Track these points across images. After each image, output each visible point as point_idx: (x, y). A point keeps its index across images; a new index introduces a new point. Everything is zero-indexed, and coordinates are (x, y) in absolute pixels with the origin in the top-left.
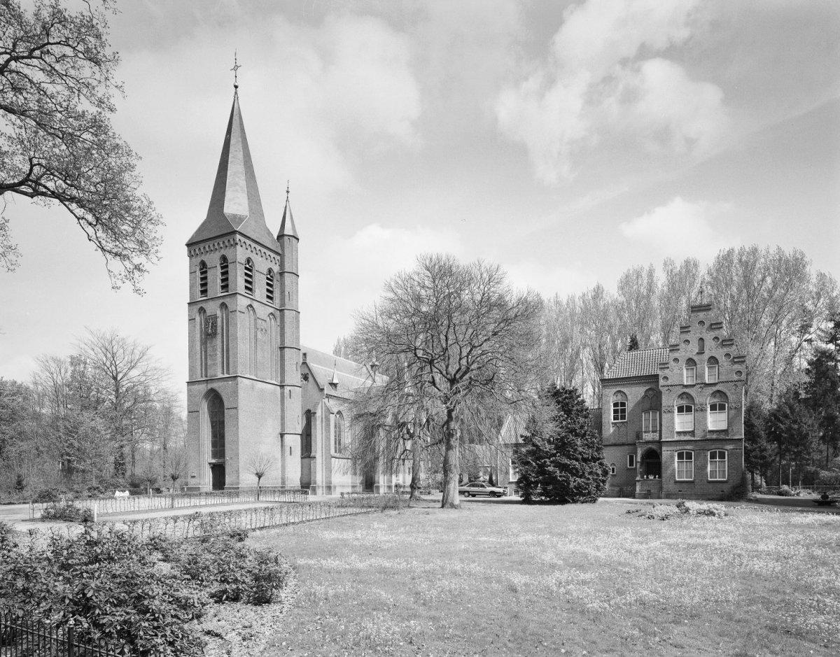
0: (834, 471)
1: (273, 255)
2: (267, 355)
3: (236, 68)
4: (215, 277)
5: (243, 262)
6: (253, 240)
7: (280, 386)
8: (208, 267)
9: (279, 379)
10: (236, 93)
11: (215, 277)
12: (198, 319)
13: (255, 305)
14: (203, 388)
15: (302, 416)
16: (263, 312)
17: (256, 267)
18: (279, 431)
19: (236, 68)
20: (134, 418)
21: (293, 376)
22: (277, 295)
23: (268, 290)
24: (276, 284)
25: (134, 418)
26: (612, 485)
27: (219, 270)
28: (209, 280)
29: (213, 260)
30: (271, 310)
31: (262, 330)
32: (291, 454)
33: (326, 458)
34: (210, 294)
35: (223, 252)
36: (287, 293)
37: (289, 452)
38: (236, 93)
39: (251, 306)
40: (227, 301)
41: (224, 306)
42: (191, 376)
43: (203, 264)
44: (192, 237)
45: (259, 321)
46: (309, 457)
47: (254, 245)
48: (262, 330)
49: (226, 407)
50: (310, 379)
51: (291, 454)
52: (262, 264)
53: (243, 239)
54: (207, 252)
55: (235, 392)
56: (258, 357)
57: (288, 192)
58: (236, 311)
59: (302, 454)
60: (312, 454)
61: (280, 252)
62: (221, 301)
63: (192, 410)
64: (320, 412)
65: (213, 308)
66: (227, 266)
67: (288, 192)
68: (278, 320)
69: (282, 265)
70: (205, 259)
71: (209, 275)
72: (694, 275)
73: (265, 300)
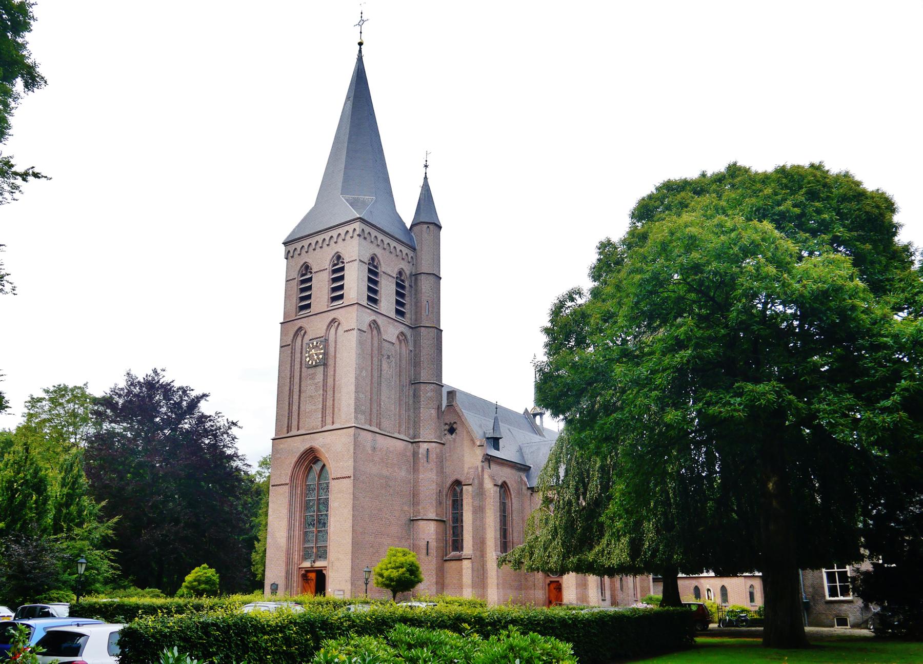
0: (23, 624)
3: (362, 22)
5: (366, 261)
6: (379, 229)
10: (360, 51)
11: (321, 285)
12: (401, 570)
13: (381, 321)
19: (362, 22)
26: (790, 402)
29: (321, 261)
30: (402, 328)
31: (388, 357)
37: (425, 551)
38: (360, 51)
43: (306, 268)
44: (294, 231)
45: (385, 344)
47: (380, 237)
48: (388, 357)
52: (390, 267)
56: (383, 398)
57: (426, 166)
62: (332, 315)
63: (458, 562)
67: (426, 166)
70: (310, 261)
72: (763, 240)
73: (393, 314)
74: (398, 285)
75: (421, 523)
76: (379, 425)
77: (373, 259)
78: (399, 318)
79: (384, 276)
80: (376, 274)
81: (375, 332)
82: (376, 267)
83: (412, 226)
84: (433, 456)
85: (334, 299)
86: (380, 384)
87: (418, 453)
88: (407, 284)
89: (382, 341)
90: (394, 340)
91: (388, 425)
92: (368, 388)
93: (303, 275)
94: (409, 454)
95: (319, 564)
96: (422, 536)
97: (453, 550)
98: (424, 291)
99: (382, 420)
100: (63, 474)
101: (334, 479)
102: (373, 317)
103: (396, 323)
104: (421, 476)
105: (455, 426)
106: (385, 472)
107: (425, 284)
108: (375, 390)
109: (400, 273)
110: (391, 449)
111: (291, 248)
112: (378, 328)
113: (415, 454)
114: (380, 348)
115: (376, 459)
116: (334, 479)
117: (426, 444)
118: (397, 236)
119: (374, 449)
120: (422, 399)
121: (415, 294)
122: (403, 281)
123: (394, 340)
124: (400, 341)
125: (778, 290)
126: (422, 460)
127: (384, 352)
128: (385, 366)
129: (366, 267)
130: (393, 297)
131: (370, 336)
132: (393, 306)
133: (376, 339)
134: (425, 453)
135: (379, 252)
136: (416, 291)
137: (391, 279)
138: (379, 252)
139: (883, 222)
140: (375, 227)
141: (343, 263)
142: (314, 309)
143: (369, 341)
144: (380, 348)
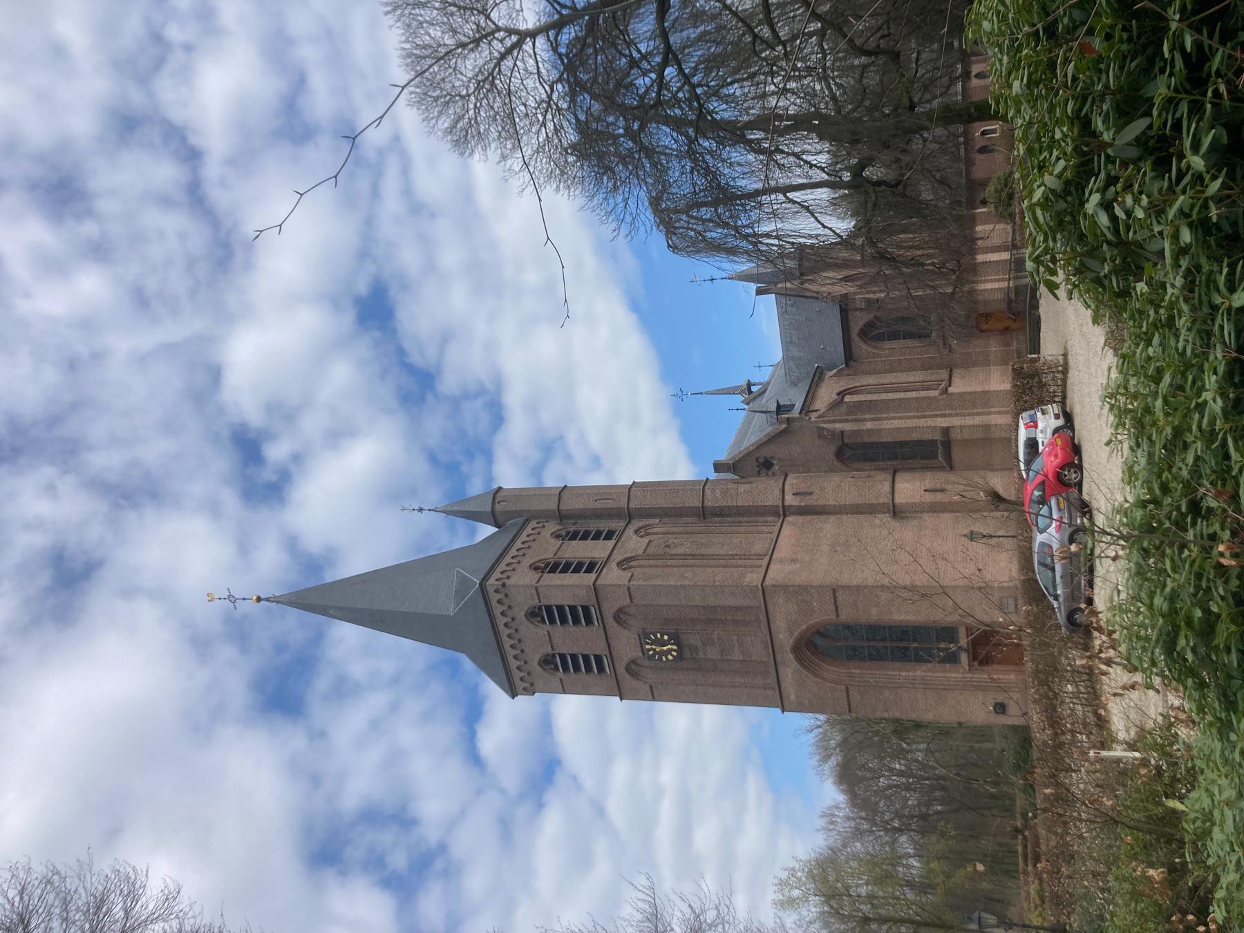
1: (528, 530)
2: (724, 542)
4: (571, 639)
7: (785, 516)
8: (549, 650)
9: (770, 519)
10: (267, 600)
11: (571, 639)
13: (618, 556)
14: (790, 671)
15: (854, 470)
16: (633, 543)
17: (549, 555)
18: (886, 518)
21: (766, 491)
22: (604, 525)
24: (581, 527)
27: (558, 630)
28: (566, 601)
29: (537, 639)
30: (630, 532)
31: (668, 546)
33: (951, 408)
34: (600, 648)
35: (520, 614)
36: (598, 505)
38: (267, 600)
39: (619, 564)
41: (620, 616)
46: (947, 445)
48: (668, 546)
49: (833, 617)
50: (766, 452)
52: (547, 546)
53: (497, 574)
54: (506, 595)
55: (798, 592)
56: (722, 552)
58: (629, 589)
59: (941, 468)
60: (937, 436)
61: (520, 520)
62: (610, 621)
66: (549, 609)
68: (651, 521)
69: (543, 516)
70: (537, 657)
71: (556, 599)
73: (611, 543)
75: (897, 500)
76: (760, 556)
77: (536, 569)
79: (559, 554)
81: (633, 563)
83: (497, 525)
84: (803, 487)
85: (589, 621)
86: (703, 556)
87: (799, 507)
88: (572, 529)
89: (646, 555)
90: (646, 540)
91: (760, 545)
92: (709, 570)
94: (800, 519)
95: (963, 642)
96: (917, 500)
97: (936, 457)
98: (581, 506)
99: (754, 552)
100: (1190, 682)
101: (837, 615)
102: (614, 565)
105: (761, 460)
107: (570, 504)
108: (712, 562)
109: (557, 537)
110: (793, 541)
111: (520, 685)
114: (655, 557)
115: (807, 558)
116: (837, 615)
117: (787, 497)
118: (507, 541)
119: (794, 561)
120: (725, 504)
122: (568, 533)
123: (646, 540)
124: (648, 534)
127: (661, 552)
128: (680, 551)
131: (639, 570)
133: (643, 562)
134: (798, 498)
135: (527, 562)
137: (564, 546)
138: (527, 562)
140: (488, 611)
141: (540, 608)
142: (601, 649)
143: (645, 570)
144: (655, 557)
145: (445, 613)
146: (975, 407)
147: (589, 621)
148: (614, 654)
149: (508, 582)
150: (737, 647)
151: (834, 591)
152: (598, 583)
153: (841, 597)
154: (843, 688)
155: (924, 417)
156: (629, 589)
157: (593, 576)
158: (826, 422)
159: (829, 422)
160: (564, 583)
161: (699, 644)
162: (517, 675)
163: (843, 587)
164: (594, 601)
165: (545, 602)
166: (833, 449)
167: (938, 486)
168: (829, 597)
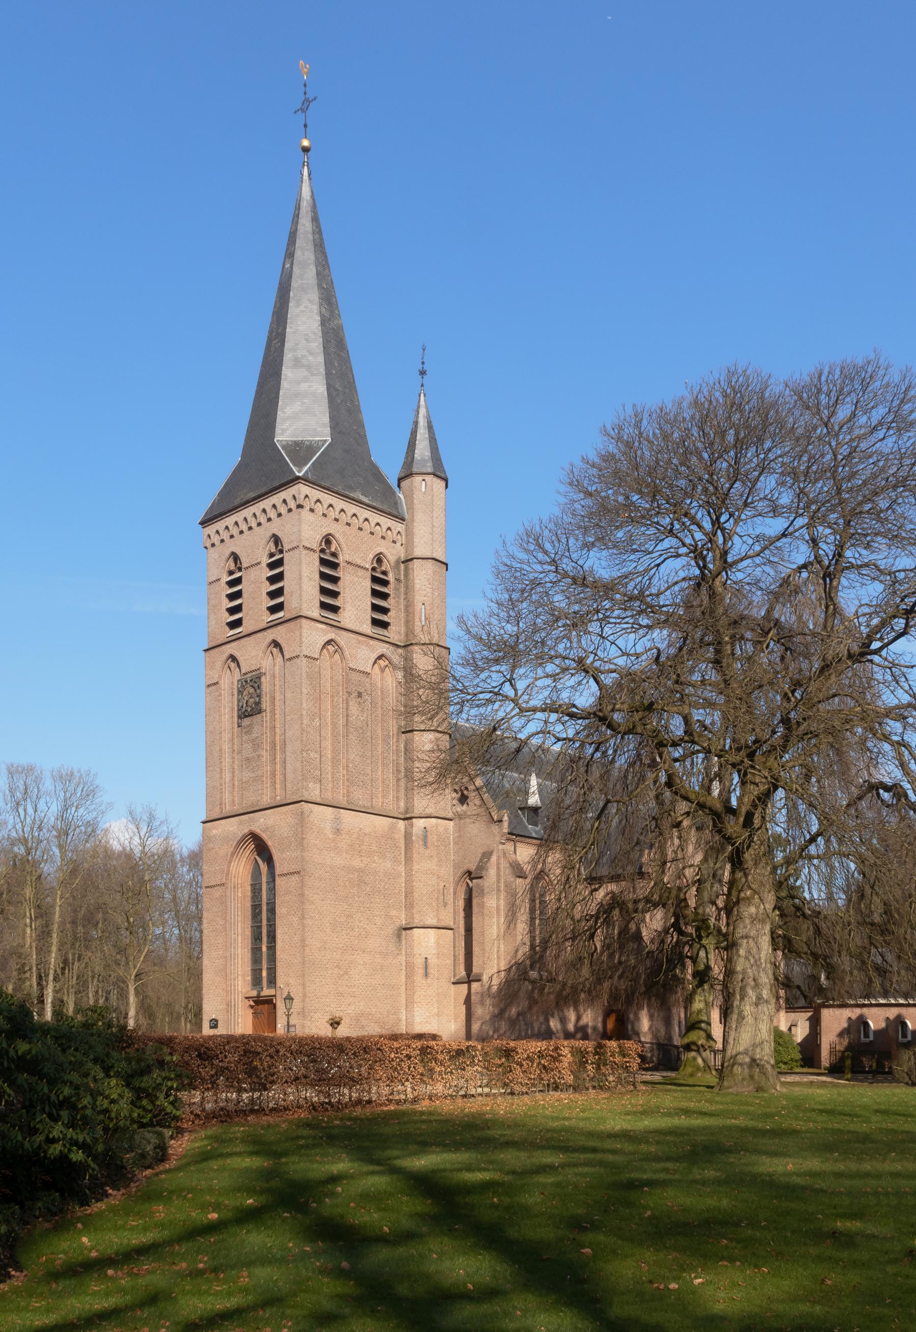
4: (256, 586)
5: (315, 546)
11: (256, 586)
13: (343, 638)
14: (235, 828)
16: (363, 655)
20: (684, 545)
23: (335, 594)
25: (684, 545)
29: (254, 549)
31: (360, 695)
32: (426, 975)
35: (275, 527)
37: (421, 971)
40: (277, 634)
42: (209, 811)
45: (355, 676)
48: (360, 695)
51: (426, 975)
55: (300, 840)
58: (298, 657)
62: (271, 635)
64: (494, 879)
65: (252, 654)
67: (423, 373)
73: (367, 628)
74: (375, 580)
78: (380, 631)
80: (335, 566)
82: (334, 555)
84: (432, 838)
85: (273, 610)
87: (411, 834)
93: (231, 573)
96: (417, 951)
98: (417, 587)
103: (372, 642)
104: (416, 867)
106: (357, 863)
109: (379, 560)
110: (367, 830)
112: (339, 650)
113: (408, 836)
119: (337, 831)
121: (406, 594)
125: (149, 1148)
126: (417, 845)
129: (315, 558)
130: (368, 600)
132: (368, 614)
135: (337, 530)
136: (407, 587)
137: (361, 572)
139: (33, 1024)
145: (278, 430)
146: (867, 996)
147: (273, 610)
148: (243, 640)
149: (305, 512)
150: (252, 775)
151: (298, 873)
152: (304, 621)
153: (295, 878)
154: (224, 881)
155: (498, 958)
156: (298, 657)
157: (316, 612)
158: (498, 858)
159: (498, 864)
160: (305, 580)
161: (254, 735)
162: (220, 525)
163: (302, 881)
164: (288, 616)
165: (287, 557)
166: (473, 868)
167: (431, 971)
168: (294, 868)
